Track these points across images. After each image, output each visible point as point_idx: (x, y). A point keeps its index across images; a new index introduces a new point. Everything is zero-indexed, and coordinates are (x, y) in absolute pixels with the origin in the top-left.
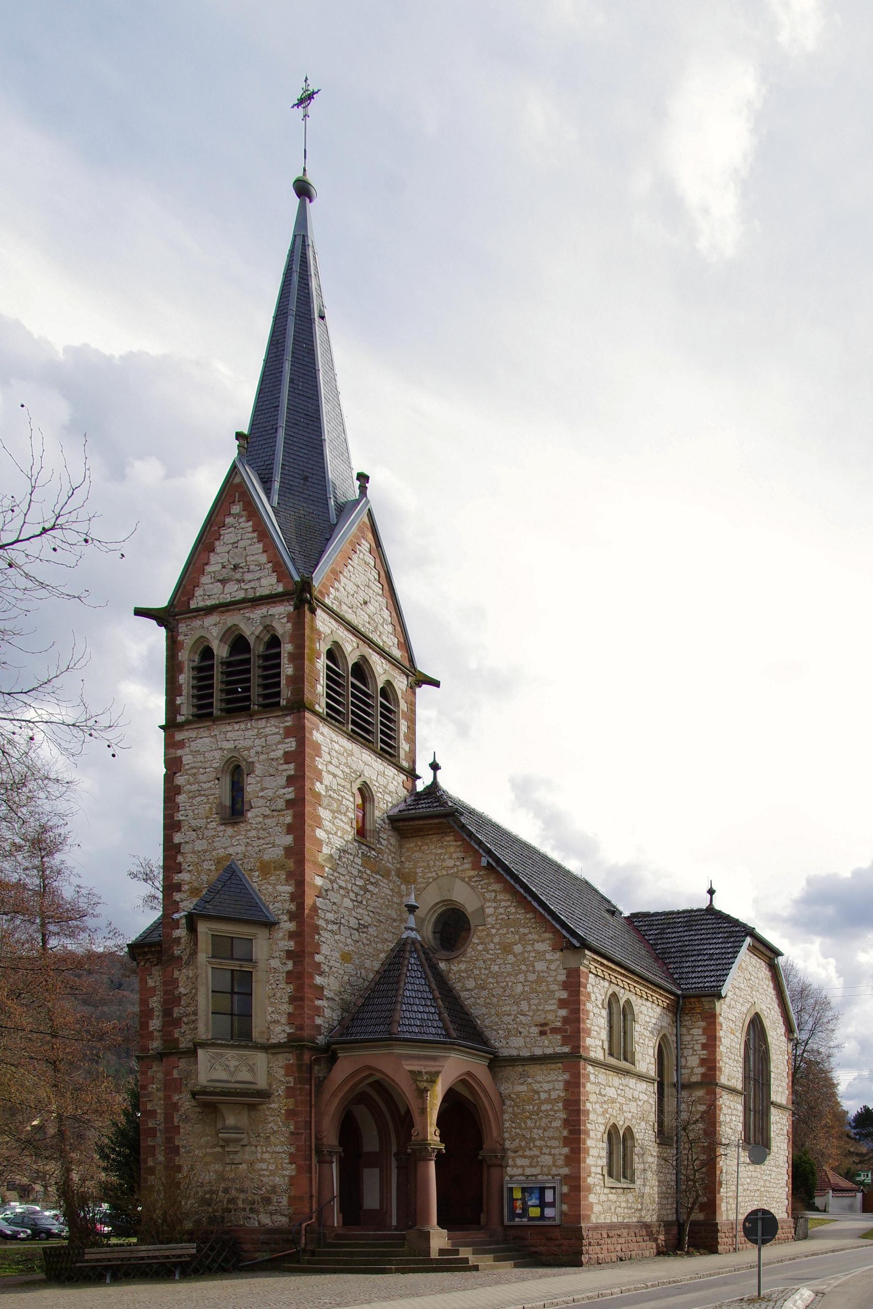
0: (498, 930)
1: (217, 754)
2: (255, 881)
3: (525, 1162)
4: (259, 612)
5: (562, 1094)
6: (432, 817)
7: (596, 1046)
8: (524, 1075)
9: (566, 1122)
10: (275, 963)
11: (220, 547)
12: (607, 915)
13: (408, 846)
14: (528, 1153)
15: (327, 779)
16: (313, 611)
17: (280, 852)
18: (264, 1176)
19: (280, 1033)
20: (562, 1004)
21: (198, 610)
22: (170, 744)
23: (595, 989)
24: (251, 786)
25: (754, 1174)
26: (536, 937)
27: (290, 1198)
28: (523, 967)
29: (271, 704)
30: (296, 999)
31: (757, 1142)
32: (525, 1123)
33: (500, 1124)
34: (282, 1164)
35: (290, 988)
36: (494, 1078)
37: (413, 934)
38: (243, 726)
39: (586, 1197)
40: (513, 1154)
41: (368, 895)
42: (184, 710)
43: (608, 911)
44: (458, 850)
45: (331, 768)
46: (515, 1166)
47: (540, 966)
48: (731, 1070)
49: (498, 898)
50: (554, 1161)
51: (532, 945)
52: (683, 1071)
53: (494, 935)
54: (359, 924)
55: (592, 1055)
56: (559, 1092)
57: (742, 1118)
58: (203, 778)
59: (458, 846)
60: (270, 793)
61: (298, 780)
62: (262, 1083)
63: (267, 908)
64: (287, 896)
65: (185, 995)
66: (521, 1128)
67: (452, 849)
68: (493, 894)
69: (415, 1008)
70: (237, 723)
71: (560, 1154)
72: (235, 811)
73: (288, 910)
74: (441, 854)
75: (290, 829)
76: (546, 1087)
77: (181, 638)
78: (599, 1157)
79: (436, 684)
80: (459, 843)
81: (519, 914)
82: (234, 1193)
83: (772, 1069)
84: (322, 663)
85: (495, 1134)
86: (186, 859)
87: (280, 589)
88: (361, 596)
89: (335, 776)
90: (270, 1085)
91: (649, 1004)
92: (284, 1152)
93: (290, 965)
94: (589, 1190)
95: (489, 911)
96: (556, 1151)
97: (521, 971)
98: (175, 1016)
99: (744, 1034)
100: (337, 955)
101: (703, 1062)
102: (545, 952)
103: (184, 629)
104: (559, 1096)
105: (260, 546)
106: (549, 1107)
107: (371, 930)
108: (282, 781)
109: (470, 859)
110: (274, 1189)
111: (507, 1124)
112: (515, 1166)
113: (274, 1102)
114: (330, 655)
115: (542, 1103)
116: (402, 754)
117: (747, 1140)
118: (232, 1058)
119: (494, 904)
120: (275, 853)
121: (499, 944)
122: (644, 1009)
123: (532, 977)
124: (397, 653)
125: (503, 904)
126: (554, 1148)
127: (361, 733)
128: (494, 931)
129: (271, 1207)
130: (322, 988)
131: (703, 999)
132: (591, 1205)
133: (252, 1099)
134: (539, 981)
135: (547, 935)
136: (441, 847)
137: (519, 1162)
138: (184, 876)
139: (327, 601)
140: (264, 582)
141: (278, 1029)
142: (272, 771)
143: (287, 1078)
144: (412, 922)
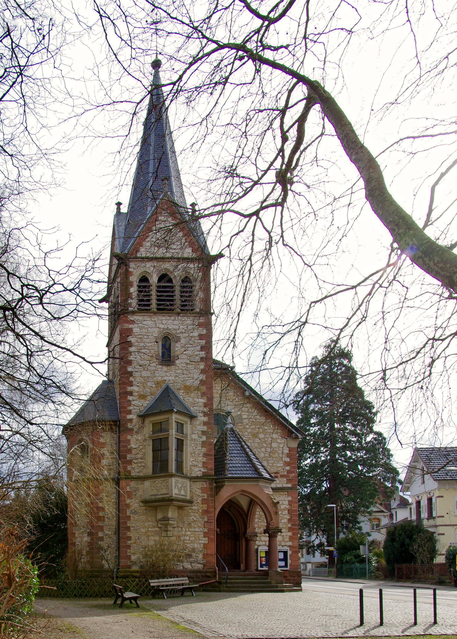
5: (287, 507)
18: (187, 543)
28: (265, 445)
29: (186, 308)
46: (261, 540)
53: (248, 428)
58: (148, 340)
64: (201, 404)
73: (202, 411)
87: (194, 255)
93: (204, 438)
97: (263, 447)
98: (128, 459)
102: (276, 439)
103: (134, 266)
108: (199, 348)
110: (193, 550)
111: (256, 520)
112: (261, 540)
113: (194, 506)
119: (247, 414)
121: (250, 433)
128: (248, 426)
129: (191, 559)
133: (183, 504)
141: (196, 469)
142: (191, 342)
143: (203, 494)
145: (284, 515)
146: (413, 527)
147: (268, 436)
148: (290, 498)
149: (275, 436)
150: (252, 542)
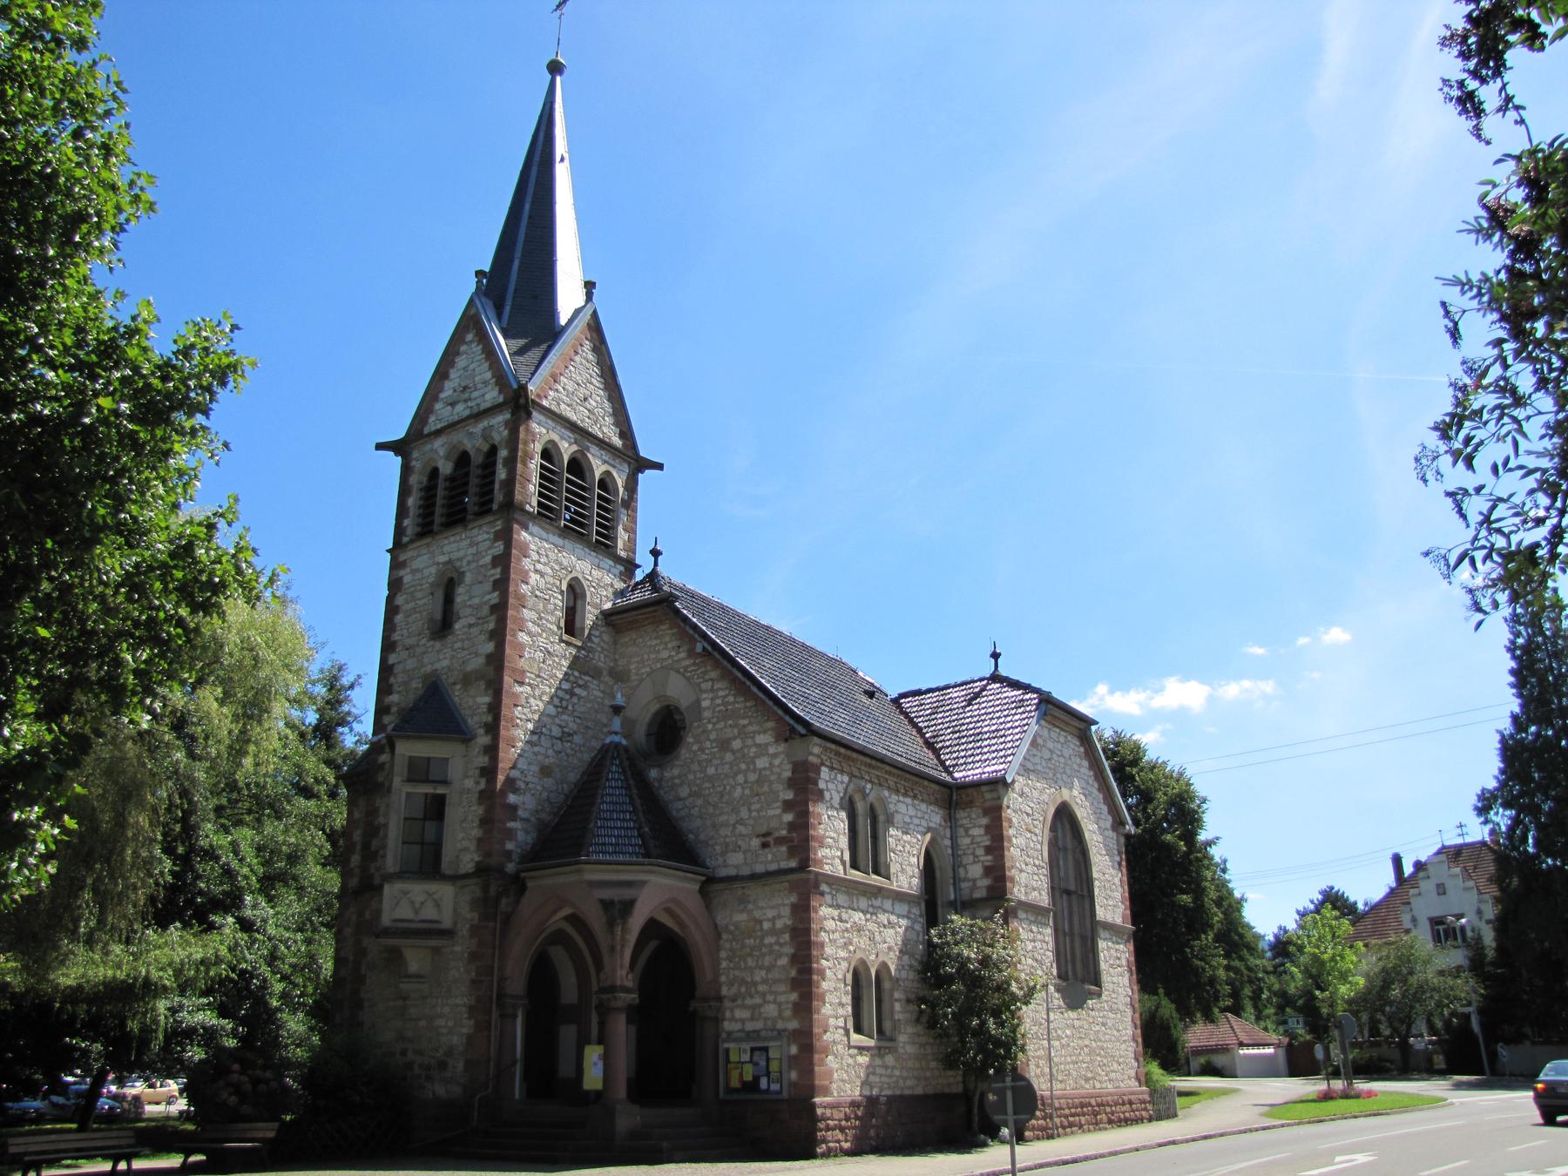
1: (433, 570)
2: (457, 695)
3: (745, 1014)
6: (656, 608)
7: (833, 858)
8: (743, 901)
9: (794, 959)
10: (469, 783)
11: (453, 374)
12: (864, 699)
14: (748, 1002)
15: (534, 577)
16: (529, 415)
17: (481, 660)
19: (468, 863)
21: (429, 435)
22: (396, 565)
23: (831, 786)
25: (1077, 1023)
28: (743, 766)
29: (484, 509)
30: (486, 822)
31: (1078, 977)
33: (716, 963)
35: (480, 811)
36: (707, 907)
37: (617, 739)
39: (822, 1063)
41: (575, 700)
42: (409, 532)
43: (866, 692)
45: (539, 566)
46: (733, 1019)
47: (762, 763)
48: (1029, 877)
50: (780, 1011)
52: (963, 885)
55: (827, 869)
56: (785, 920)
57: (1051, 945)
60: (476, 601)
61: (502, 584)
62: (447, 923)
63: (465, 722)
64: (484, 708)
69: (612, 824)
72: (443, 626)
76: (770, 914)
77: (414, 463)
78: (842, 1005)
79: (660, 466)
82: (410, 1055)
83: (1095, 875)
84: (535, 463)
86: (396, 680)
88: (582, 392)
89: (542, 575)
90: (455, 923)
91: (909, 800)
94: (826, 1051)
95: (705, 704)
96: (782, 998)
99: (1047, 831)
100: (535, 768)
101: (988, 871)
102: (767, 745)
105: (486, 365)
107: (577, 739)
108: (488, 586)
110: (450, 1052)
111: (724, 964)
112: (733, 1019)
114: (546, 454)
116: (620, 544)
117: (1062, 976)
118: (418, 890)
120: (477, 663)
122: (902, 808)
123: (752, 777)
124: (617, 442)
125: (721, 693)
127: (575, 531)
128: (710, 726)
130: (514, 808)
132: (830, 1073)
134: (760, 781)
135: (771, 724)
137: (739, 1014)
138: (394, 698)
139: (545, 403)
140: (488, 397)
144: (617, 723)
146: (49, 968)
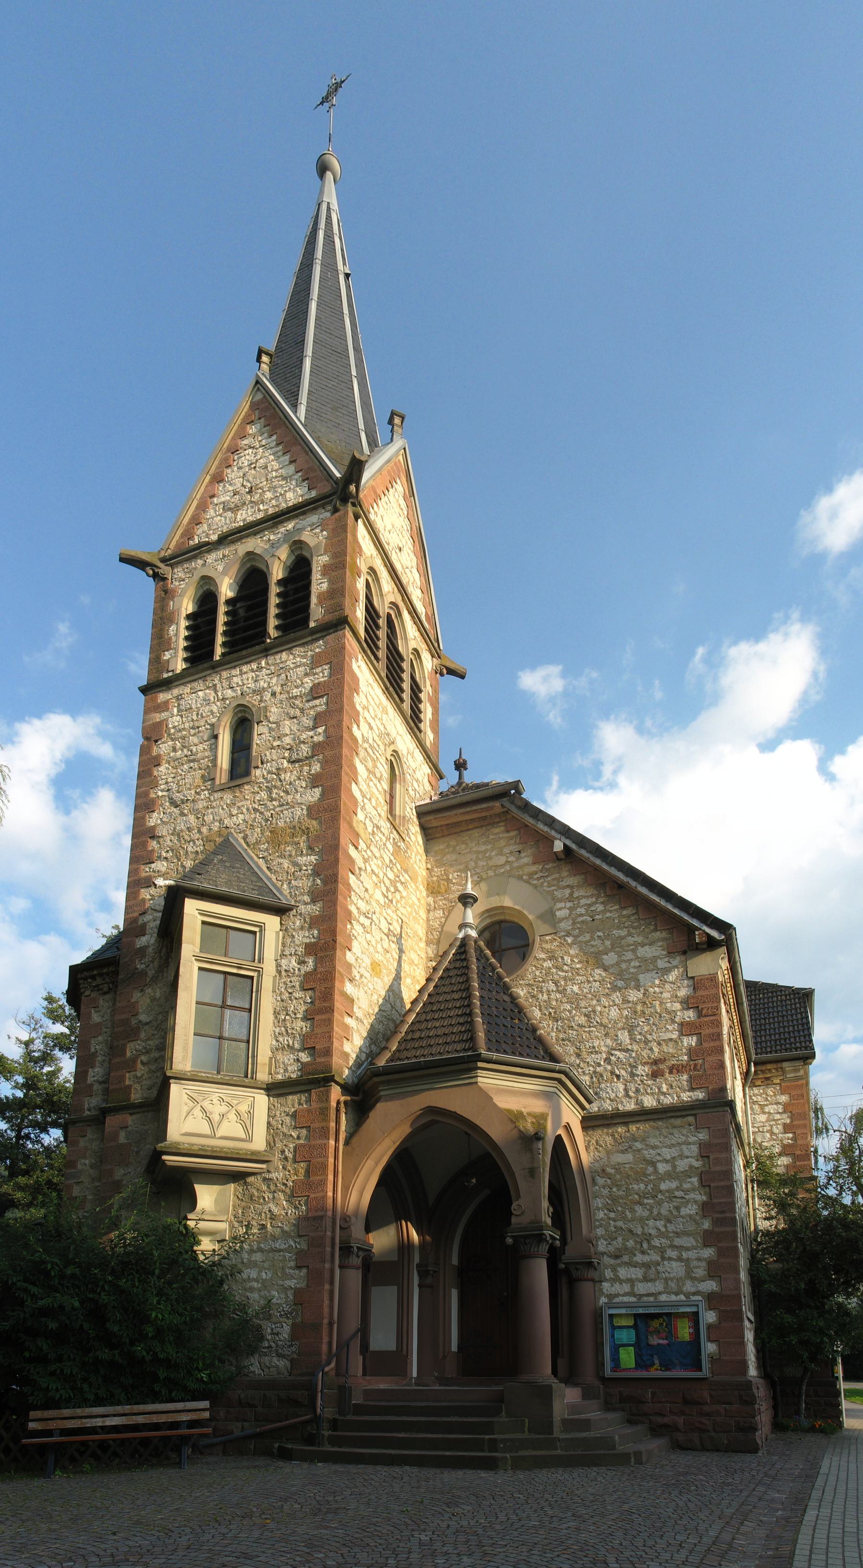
0: (576, 937)
3: (637, 1273)
4: (282, 530)
5: (697, 1164)
9: (706, 1208)
13: (436, 848)
14: (639, 1258)
17: (300, 812)
18: (252, 1289)
20: (686, 1028)
24: (260, 736)
26: (639, 939)
27: (294, 1327)
32: (632, 1211)
34: (283, 1269)
38: (254, 666)
40: (612, 1261)
44: (512, 842)
49: (576, 895)
51: (634, 951)
54: (389, 930)
56: (691, 1159)
59: (511, 838)
65: (147, 1024)
66: (624, 1219)
67: (502, 843)
68: (567, 891)
70: (247, 663)
71: (699, 1259)
74: (485, 852)
75: (314, 781)
76: (667, 1153)
80: (513, 834)
81: (611, 911)
85: (585, 1231)
92: (289, 1250)
96: (692, 1254)
102: (654, 959)
104: (691, 1166)
106: (674, 1185)
109: (529, 852)
111: (601, 1215)
112: (616, 1279)
115: (662, 1179)
119: (569, 905)
125: (583, 901)
126: (688, 1249)
131: (785, 1064)
135: (658, 935)
136: (484, 843)
137: (623, 1273)
139: (372, 517)
145: (686, 1191)
147: (629, 955)
148: (703, 1136)
149: (646, 952)
150: (586, 1288)
